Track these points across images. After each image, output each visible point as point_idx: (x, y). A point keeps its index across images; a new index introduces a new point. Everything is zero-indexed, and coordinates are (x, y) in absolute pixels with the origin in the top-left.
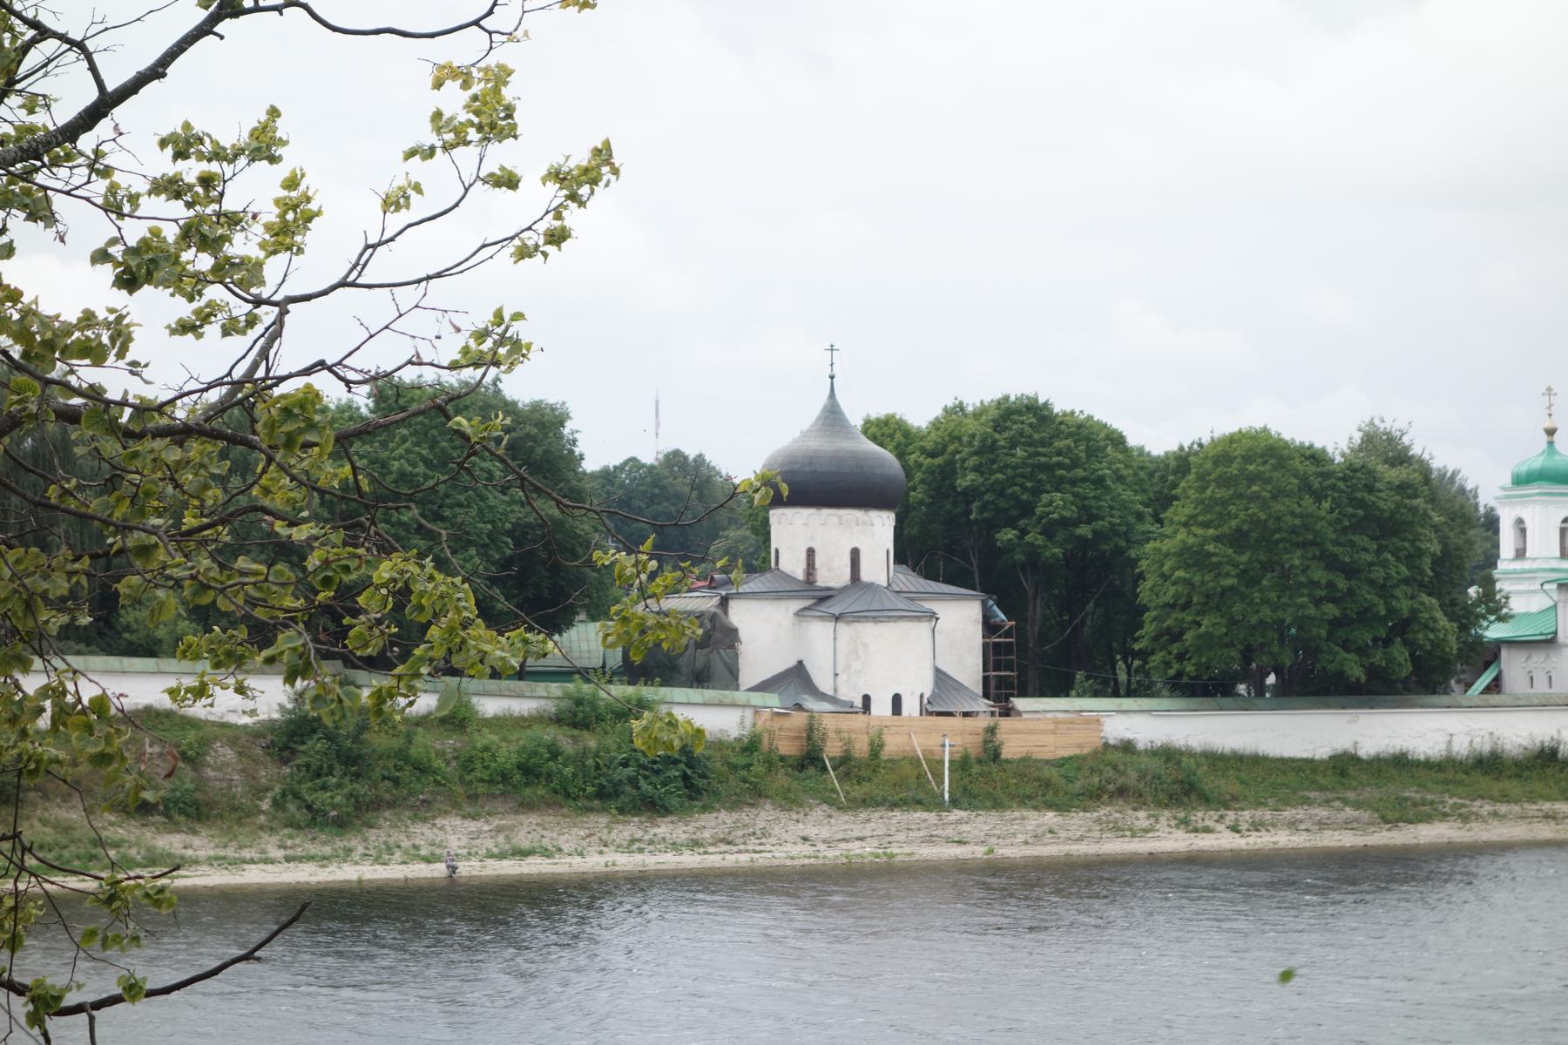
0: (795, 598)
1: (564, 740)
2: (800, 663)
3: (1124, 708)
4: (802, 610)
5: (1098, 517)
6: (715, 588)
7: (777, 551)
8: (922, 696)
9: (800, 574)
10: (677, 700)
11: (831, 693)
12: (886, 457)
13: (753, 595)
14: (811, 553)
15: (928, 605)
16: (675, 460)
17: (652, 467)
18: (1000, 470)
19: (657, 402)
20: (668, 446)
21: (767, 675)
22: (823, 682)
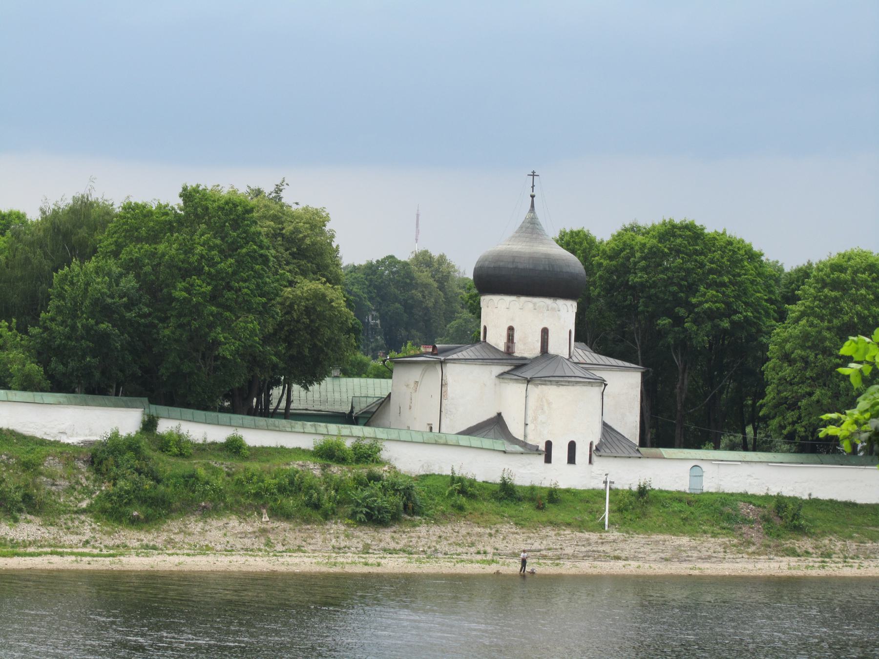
0: (498, 364)
1: (314, 469)
2: (499, 415)
3: (747, 459)
4: (502, 374)
5: (736, 312)
6: (436, 354)
7: (485, 328)
8: (591, 444)
9: (502, 347)
10: (461, 443)
11: (521, 438)
12: (572, 261)
13: (466, 360)
14: (511, 329)
15: (599, 374)
16: (424, 260)
17: (405, 264)
18: (662, 272)
19: (418, 215)
20: (418, 248)
21: (473, 423)
22: (515, 429)
